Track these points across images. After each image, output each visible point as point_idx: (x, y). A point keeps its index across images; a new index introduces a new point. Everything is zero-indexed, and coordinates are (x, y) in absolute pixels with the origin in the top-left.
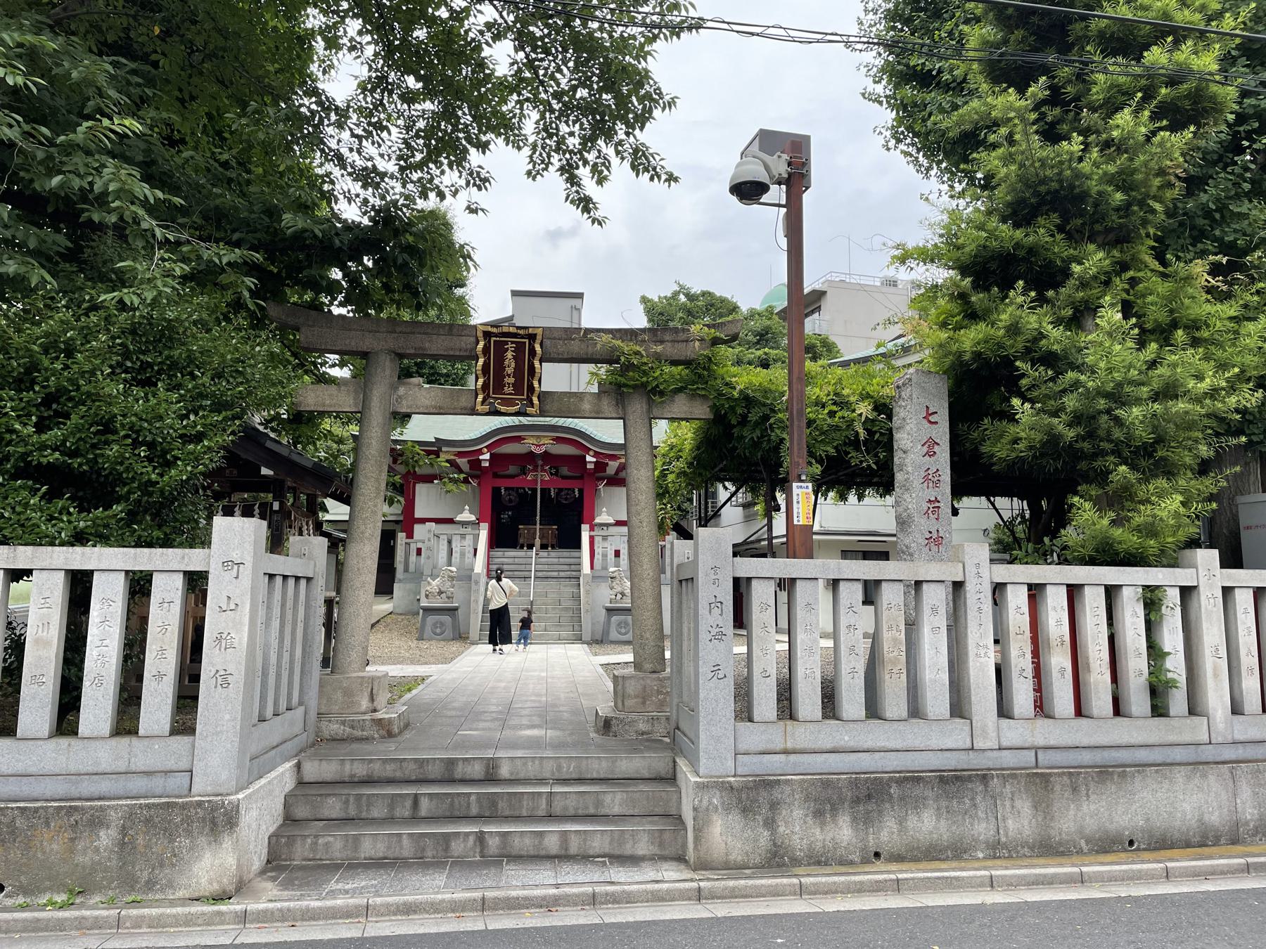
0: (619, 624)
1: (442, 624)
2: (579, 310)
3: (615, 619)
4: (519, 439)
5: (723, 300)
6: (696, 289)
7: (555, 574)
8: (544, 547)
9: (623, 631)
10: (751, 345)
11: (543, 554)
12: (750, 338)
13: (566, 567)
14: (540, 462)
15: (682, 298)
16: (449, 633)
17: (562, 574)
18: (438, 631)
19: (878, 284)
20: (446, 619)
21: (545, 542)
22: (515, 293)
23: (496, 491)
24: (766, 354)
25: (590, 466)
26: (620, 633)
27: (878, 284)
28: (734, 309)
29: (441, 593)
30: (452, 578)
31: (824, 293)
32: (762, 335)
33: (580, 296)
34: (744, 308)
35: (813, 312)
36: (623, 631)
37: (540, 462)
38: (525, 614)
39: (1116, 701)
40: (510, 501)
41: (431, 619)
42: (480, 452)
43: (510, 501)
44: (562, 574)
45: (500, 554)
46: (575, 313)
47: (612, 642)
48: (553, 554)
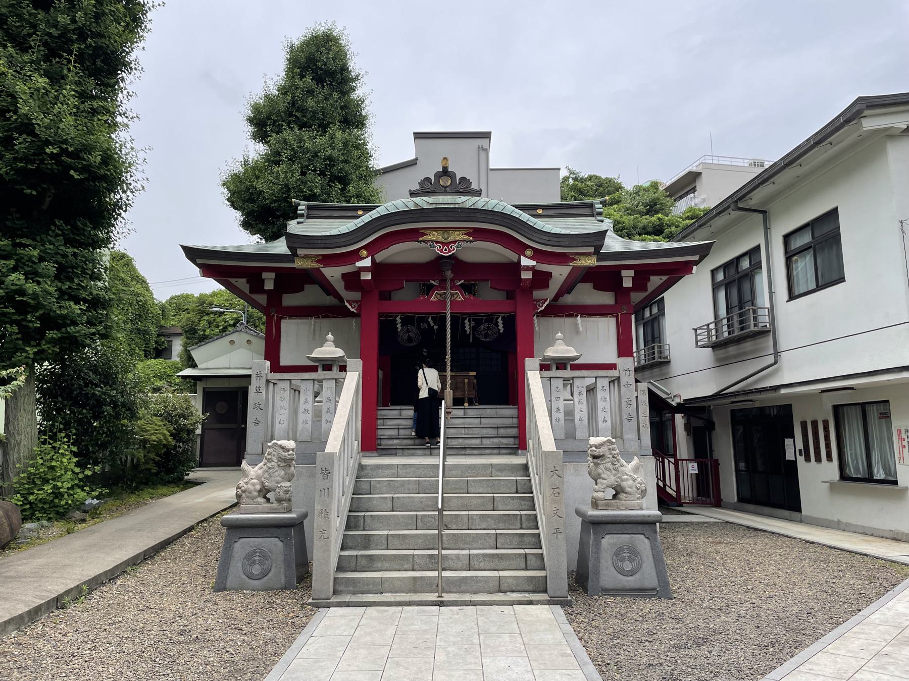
0: (618, 553)
1: (264, 555)
2: (486, 151)
3: (609, 542)
4: (414, 235)
5: (609, 181)
6: (585, 174)
7: (476, 442)
8: (458, 402)
9: (628, 566)
10: (642, 214)
11: (458, 412)
12: (641, 208)
13: (492, 432)
14: (449, 274)
15: (571, 181)
16: (278, 574)
17: (487, 442)
18: (256, 570)
19: (747, 165)
20: (273, 545)
21: (459, 394)
22: (418, 136)
23: (386, 326)
24: (659, 219)
25: (526, 275)
26: (622, 572)
27: (747, 165)
28: (618, 188)
29: (264, 492)
30: (286, 463)
31: (701, 173)
32: (651, 207)
33: (487, 135)
34: (629, 185)
35: (687, 194)
36: (628, 566)
37: (449, 274)
38: (474, 186)
39: (571, 452)
40: (410, 339)
41: (244, 545)
42: (356, 255)
43: (410, 339)
44: (487, 442)
45: (395, 413)
46: (482, 154)
47: (607, 592)
48: (471, 412)
